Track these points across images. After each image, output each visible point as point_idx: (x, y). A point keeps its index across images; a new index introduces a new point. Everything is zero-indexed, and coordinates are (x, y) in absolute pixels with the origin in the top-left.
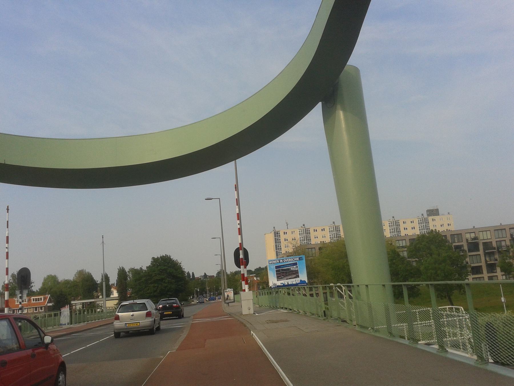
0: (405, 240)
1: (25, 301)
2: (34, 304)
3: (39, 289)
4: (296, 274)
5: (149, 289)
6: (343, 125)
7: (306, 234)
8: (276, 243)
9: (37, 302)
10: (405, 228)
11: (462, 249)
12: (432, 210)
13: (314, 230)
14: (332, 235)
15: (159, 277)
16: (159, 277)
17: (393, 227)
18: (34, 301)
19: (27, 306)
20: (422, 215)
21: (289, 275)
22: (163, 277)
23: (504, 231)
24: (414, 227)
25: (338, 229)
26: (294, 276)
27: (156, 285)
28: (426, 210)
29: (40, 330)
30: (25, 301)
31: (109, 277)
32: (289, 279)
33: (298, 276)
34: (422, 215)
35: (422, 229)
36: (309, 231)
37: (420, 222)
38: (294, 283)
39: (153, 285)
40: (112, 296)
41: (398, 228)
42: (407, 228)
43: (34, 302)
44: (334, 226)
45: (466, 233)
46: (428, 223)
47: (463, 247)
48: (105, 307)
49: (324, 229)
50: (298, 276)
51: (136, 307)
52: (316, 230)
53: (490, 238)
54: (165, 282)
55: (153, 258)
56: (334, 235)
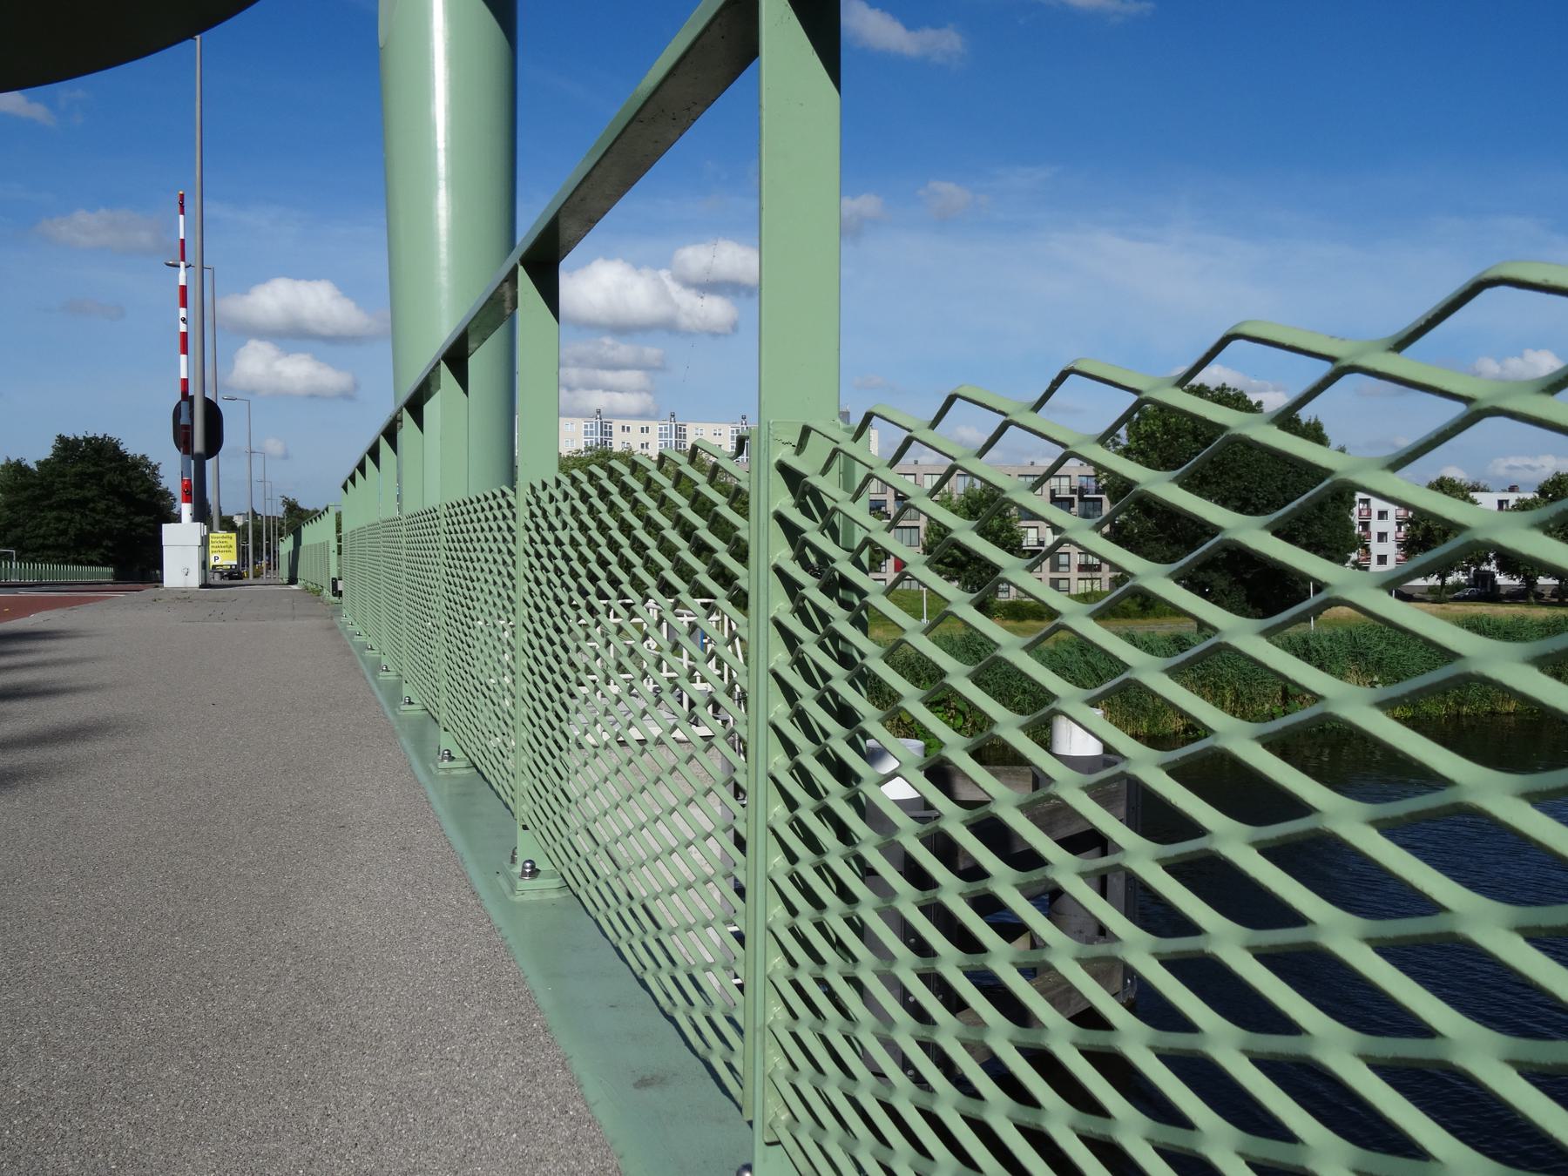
0: (1070, 476)
3: (38, 463)
5: (39, 526)
6: (1541, 1154)
11: (883, 509)
13: (623, 427)
15: (78, 494)
16: (78, 494)
17: (669, 439)
22: (89, 494)
25: (608, 430)
27: (66, 515)
31: (143, 457)
35: (666, 435)
36: (611, 427)
39: (55, 513)
41: (680, 444)
47: (885, 506)
48: (269, 497)
49: (647, 428)
52: (628, 428)
54: (93, 510)
55: (61, 439)
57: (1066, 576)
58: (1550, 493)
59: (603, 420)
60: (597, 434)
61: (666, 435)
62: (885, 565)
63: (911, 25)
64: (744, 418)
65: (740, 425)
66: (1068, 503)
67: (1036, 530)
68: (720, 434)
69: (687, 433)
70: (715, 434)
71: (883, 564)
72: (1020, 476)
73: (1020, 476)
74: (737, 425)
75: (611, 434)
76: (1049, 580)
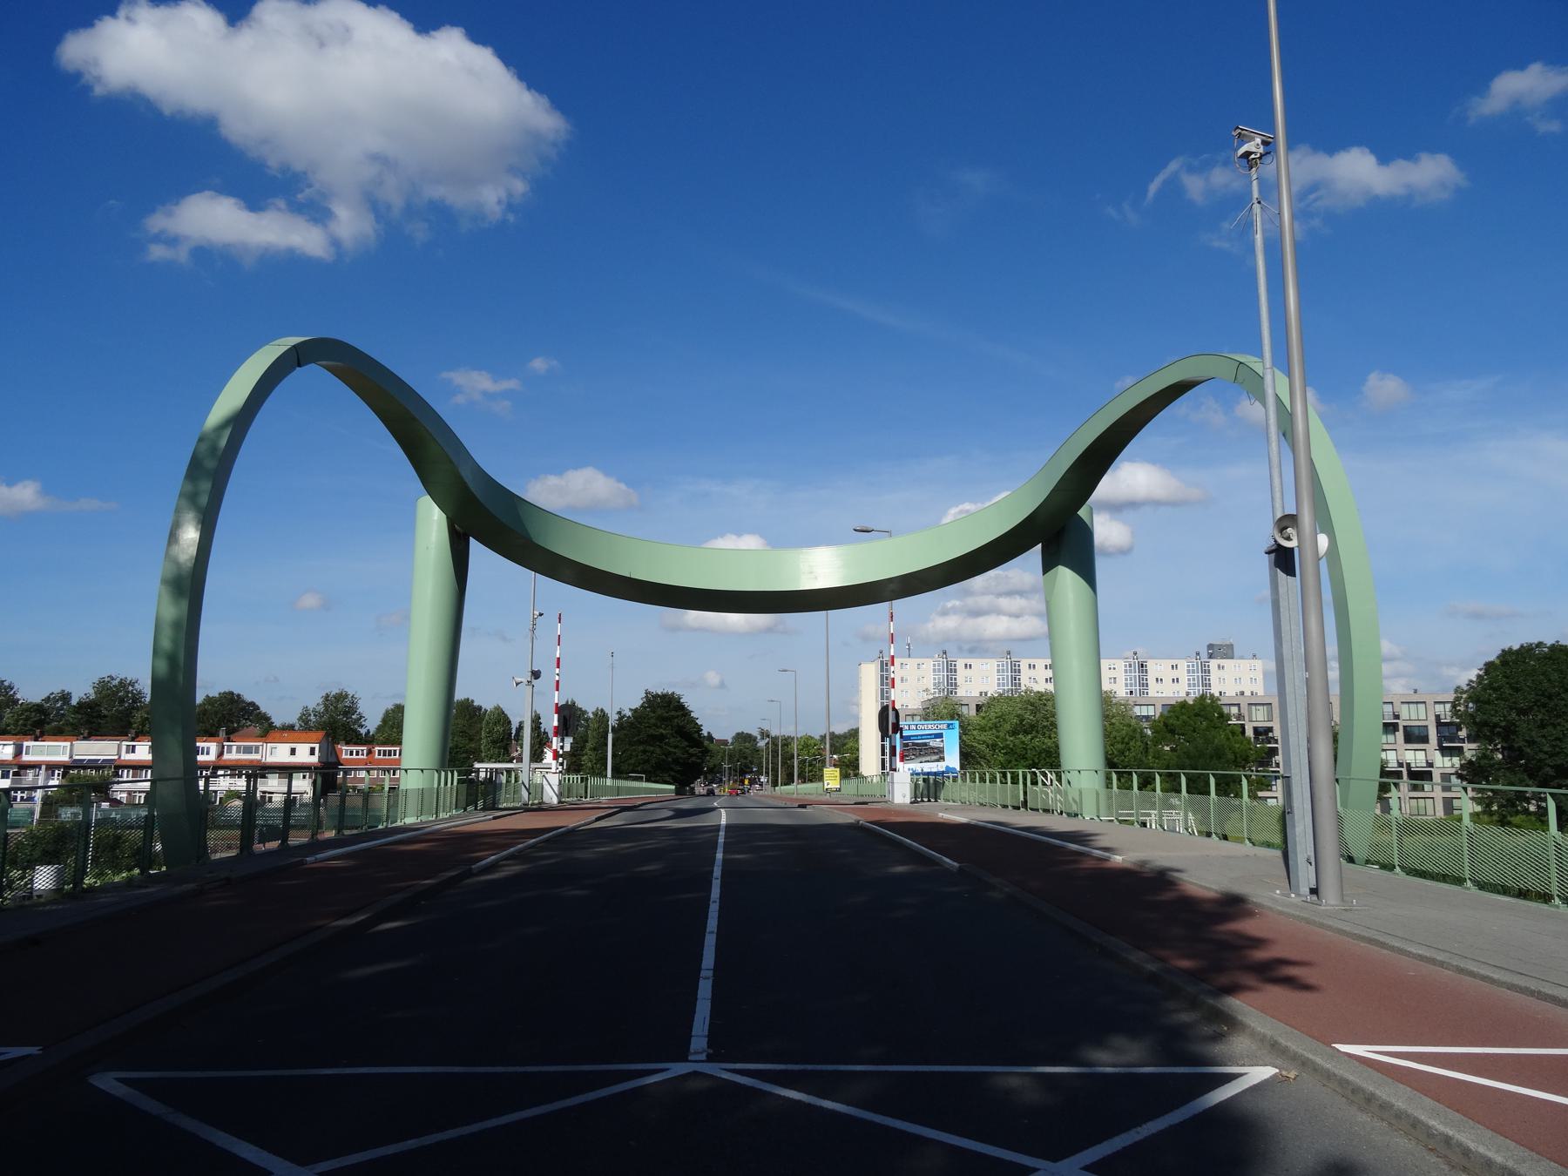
0: (1424, 702)
1: (363, 755)
2: (379, 762)
4: (939, 754)
7: (947, 672)
8: (882, 684)
9: (387, 757)
10: (1157, 679)
11: (1270, 735)
12: (1220, 647)
13: (966, 665)
14: (1003, 679)
18: (379, 755)
19: (366, 764)
20: (1198, 654)
21: (926, 754)
23: (1422, 706)
24: (1178, 679)
25: (1145, 682)
26: (936, 757)
28: (1208, 643)
29: (641, 808)
30: (363, 755)
32: (926, 762)
33: (942, 759)
34: (1198, 654)
35: (1131, 671)
36: (1019, 666)
37: (1191, 668)
38: (934, 770)
39: (641, 748)
40: (544, 761)
42: (1161, 680)
43: (349, 757)
44: (1009, 660)
45: (1436, 703)
46: (955, 672)
47: (1272, 732)
50: (942, 759)
51: (571, 782)
53: (1425, 718)
55: (207, 696)
56: (1198, 680)
57: (1431, 795)
58: (1499, 763)
59: (1203, 660)
60: (1007, 672)
61: (1131, 671)
62: (1276, 785)
63: (1384, 159)
64: (1135, 654)
65: (1132, 660)
66: (1391, 728)
67: (1423, 752)
68: (1114, 669)
69: (1021, 668)
70: (1110, 669)
71: (1274, 783)
72: (1402, 703)
73: (1402, 703)
74: (1002, 660)
75: (1019, 672)
76: (1441, 800)
